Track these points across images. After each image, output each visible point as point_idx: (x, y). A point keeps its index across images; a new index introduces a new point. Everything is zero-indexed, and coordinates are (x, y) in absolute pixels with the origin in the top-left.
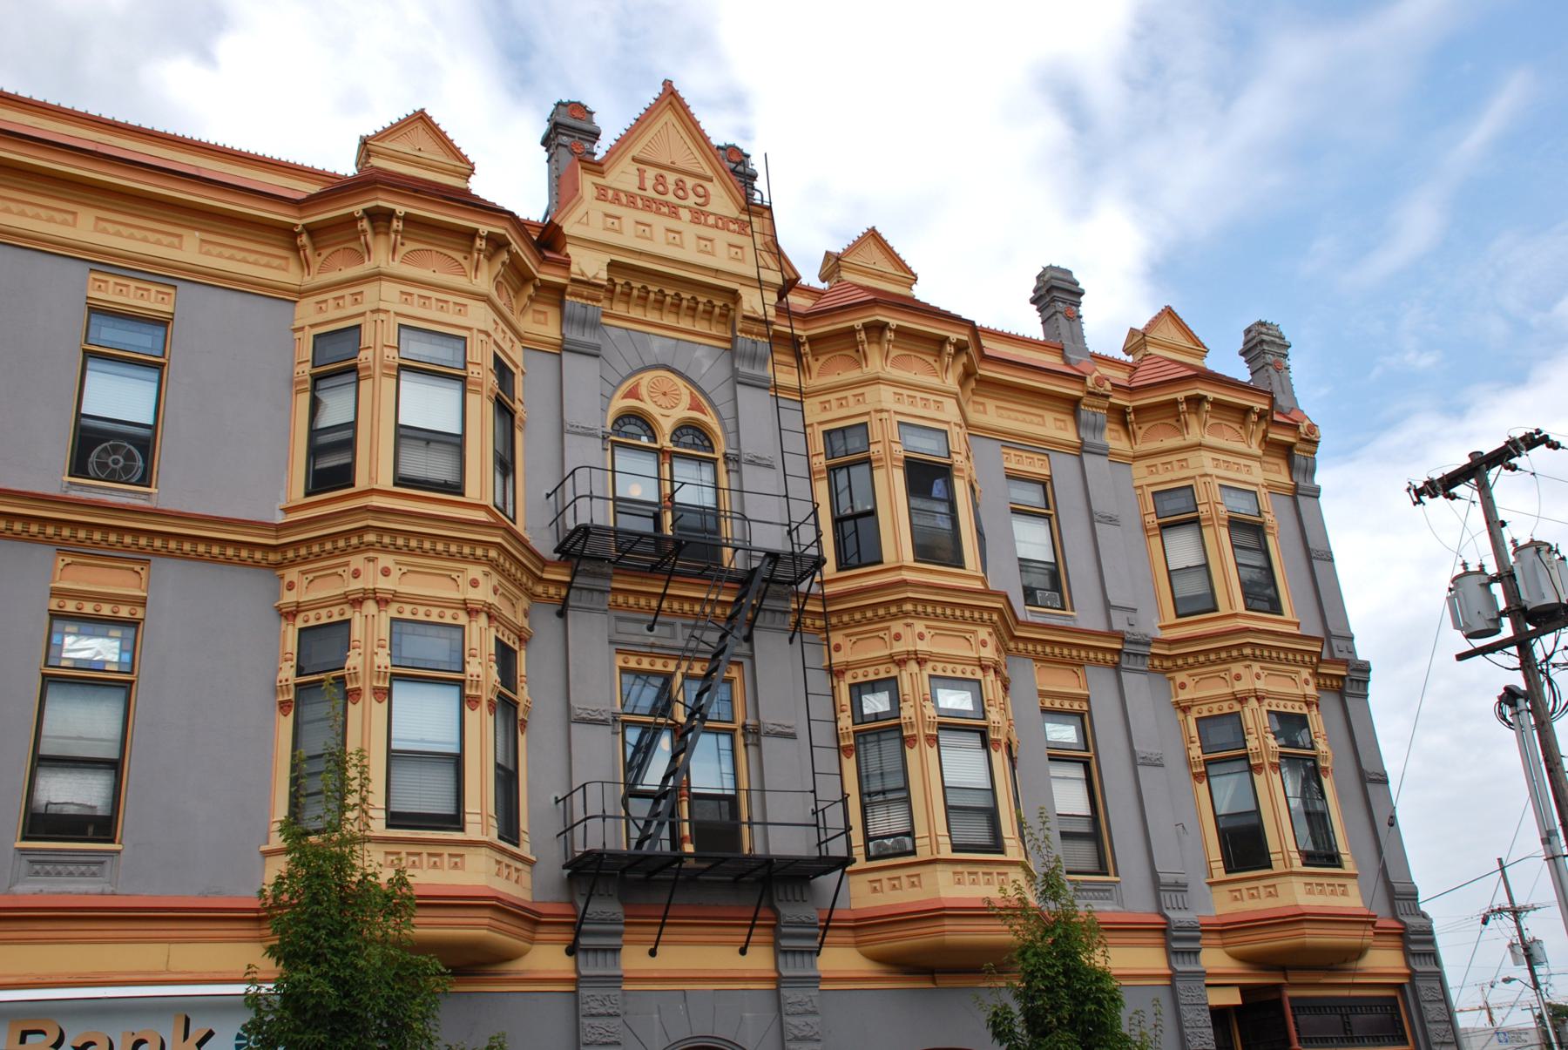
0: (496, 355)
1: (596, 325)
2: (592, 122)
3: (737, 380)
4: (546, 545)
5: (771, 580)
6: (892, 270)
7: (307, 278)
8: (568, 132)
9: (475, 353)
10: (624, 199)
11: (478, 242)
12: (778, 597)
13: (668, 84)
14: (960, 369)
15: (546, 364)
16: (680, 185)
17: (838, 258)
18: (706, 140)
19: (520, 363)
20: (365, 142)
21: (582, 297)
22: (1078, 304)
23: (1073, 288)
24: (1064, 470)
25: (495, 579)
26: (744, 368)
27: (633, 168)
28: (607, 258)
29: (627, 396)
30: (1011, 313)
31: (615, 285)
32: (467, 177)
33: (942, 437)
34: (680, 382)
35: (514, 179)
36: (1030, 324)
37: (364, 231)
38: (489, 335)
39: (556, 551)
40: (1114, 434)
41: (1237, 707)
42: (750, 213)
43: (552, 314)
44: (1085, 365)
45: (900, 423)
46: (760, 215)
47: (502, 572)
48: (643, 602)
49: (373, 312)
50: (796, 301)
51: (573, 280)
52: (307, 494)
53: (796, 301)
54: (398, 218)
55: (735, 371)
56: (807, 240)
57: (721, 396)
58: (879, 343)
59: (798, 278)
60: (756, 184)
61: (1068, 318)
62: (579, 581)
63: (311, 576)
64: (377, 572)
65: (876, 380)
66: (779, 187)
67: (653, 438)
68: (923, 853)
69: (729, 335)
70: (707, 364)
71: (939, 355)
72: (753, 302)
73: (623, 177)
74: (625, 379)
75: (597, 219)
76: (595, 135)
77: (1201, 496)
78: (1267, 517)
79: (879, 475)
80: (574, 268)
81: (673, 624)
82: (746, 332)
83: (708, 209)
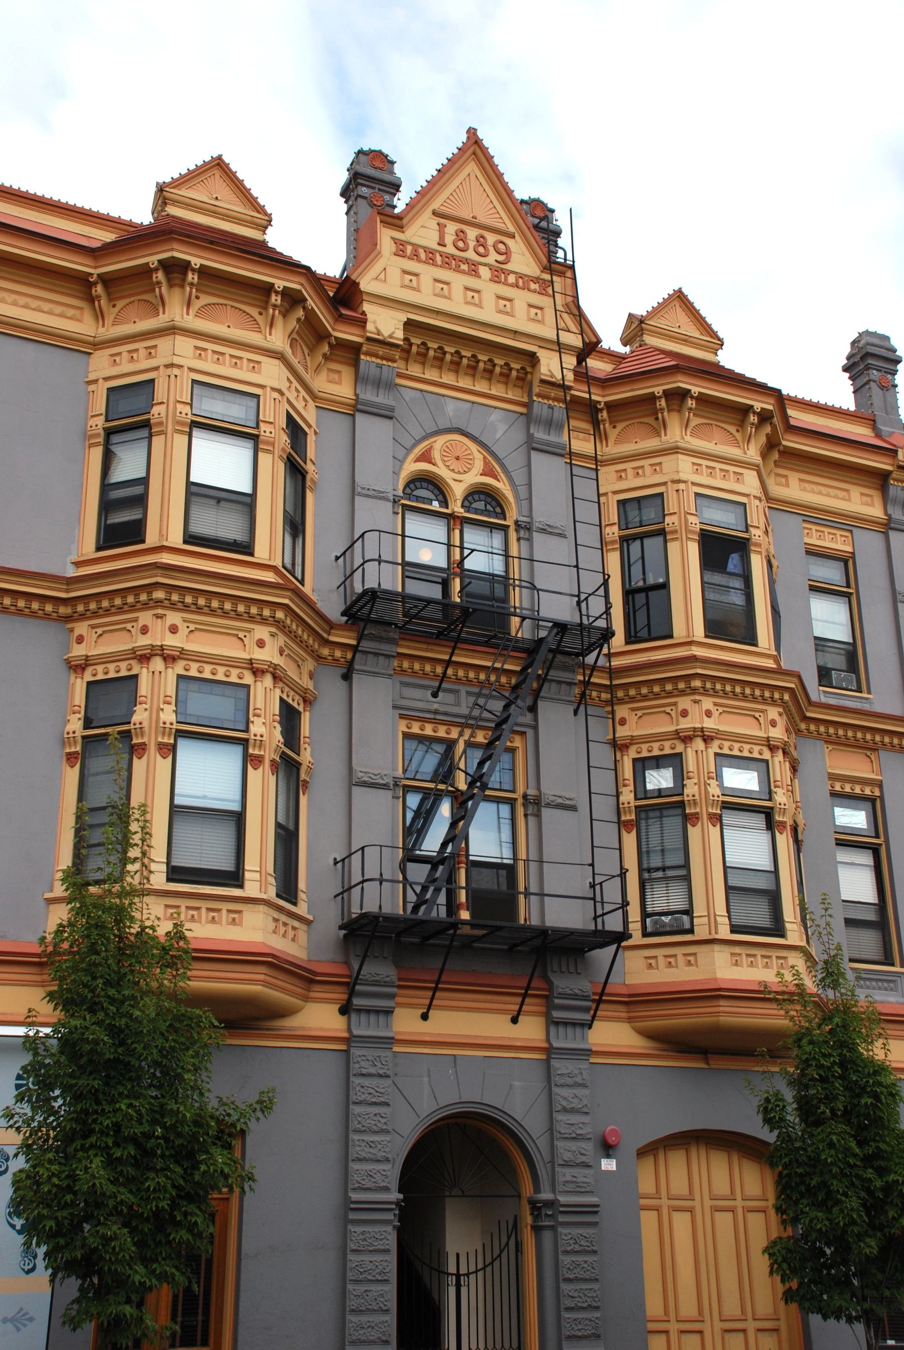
0: (289, 415)
1: (391, 386)
2: (392, 173)
3: (532, 446)
4: (333, 608)
6: (697, 334)
8: (369, 182)
9: (267, 413)
10: (423, 256)
12: (565, 668)
13: (472, 133)
14: (763, 440)
16: (481, 241)
17: (642, 321)
18: (510, 193)
20: (161, 189)
21: (377, 356)
22: (894, 372)
23: (889, 355)
24: (868, 547)
25: (282, 639)
26: (540, 434)
28: (403, 317)
34: (473, 447)
36: (840, 393)
38: (281, 393)
39: (343, 614)
41: (680, 748)
42: (552, 272)
43: (347, 374)
45: (697, 494)
46: (562, 274)
48: (428, 668)
50: (594, 364)
51: (369, 339)
52: (99, 549)
53: (594, 364)
57: (515, 462)
59: (599, 341)
61: (882, 388)
62: (365, 645)
63: (100, 631)
65: (675, 450)
66: (581, 245)
68: (701, 933)
69: (525, 400)
70: (501, 428)
71: (741, 424)
72: (551, 365)
73: (424, 231)
75: (394, 275)
80: (370, 327)
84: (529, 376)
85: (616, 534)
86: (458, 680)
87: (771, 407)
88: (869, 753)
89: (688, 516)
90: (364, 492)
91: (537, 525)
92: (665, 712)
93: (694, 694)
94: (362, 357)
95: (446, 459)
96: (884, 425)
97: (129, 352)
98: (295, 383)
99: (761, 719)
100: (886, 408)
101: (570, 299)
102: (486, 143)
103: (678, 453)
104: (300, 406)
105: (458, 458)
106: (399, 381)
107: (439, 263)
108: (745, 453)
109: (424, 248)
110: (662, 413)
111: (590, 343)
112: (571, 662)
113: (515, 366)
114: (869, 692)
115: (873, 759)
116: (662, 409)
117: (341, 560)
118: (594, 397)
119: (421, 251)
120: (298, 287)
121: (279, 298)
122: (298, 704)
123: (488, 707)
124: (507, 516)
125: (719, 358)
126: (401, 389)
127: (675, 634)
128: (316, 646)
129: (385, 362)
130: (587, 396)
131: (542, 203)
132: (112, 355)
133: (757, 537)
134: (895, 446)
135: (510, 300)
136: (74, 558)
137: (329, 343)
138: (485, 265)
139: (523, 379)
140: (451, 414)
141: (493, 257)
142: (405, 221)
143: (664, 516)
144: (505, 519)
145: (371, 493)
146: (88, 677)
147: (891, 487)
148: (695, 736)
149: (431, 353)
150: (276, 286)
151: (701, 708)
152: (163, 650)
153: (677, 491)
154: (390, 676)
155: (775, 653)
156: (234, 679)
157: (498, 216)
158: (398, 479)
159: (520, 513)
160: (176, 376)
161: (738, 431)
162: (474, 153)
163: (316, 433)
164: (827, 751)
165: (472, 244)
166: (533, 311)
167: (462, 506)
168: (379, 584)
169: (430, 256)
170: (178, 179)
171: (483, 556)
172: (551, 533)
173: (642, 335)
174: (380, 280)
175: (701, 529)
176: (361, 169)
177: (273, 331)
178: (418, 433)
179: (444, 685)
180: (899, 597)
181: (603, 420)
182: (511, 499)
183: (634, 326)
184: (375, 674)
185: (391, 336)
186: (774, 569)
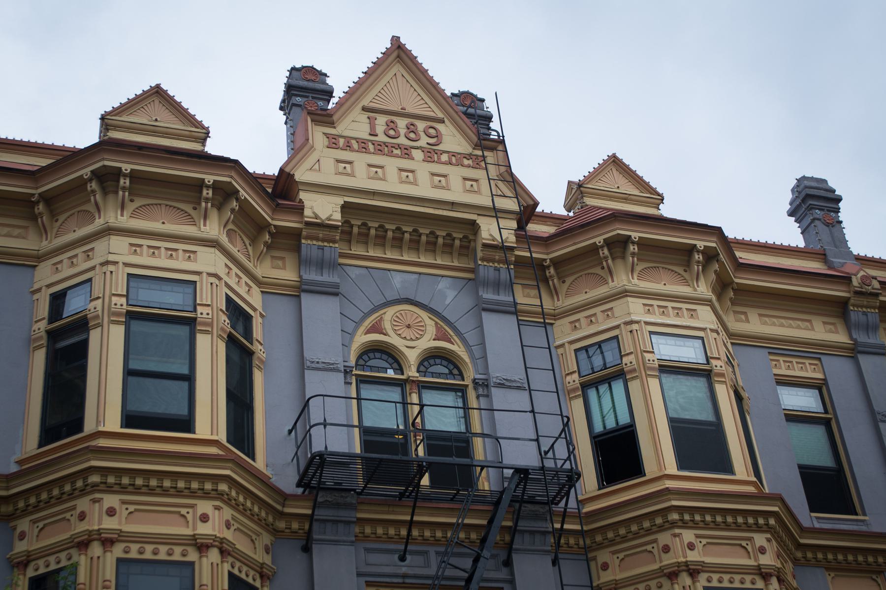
0: (228, 298)
1: (334, 266)
2: (325, 83)
4: (288, 482)
5: (519, 501)
6: (636, 192)
7: (45, 243)
8: (305, 93)
9: (204, 296)
10: (355, 146)
11: (205, 192)
12: (536, 517)
13: (395, 40)
15: (283, 308)
16: (411, 128)
17: (580, 185)
18: (441, 92)
19: (260, 309)
20: (103, 118)
21: (317, 239)
22: (837, 210)
23: (829, 195)
25: (228, 513)
26: (488, 295)
27: (364, 117)
28: (340, 201)
30: (763, 220)
31: (352, 226)
34: (424, 315)
35: (251, 135)
36: (791, 234)
37: (93, 191)
38: (220, 278)
39: (299, 485)
42: (484, 148)
43: (290, 260)
44: (850, 267)
45: (651, 333)
46: (492, 149)
47: (236, 506)
48: (392, 531)
50: (535, 228)
51: (308, 224)
52: (40, 445)
53: (535, 228)
54: (698, 251)
55: (518, 320)
56: (548, 177)
57: (466, 325)
58: (623, 258)
59: (536, 204)
60: (492, 125)
61: (827, 225)
62: (321, 513)
63: (41, 525)
64: (108, 513)
65: (624, 293)
66: (511, 124)
69: (472, 266)
70: (450, 294)
71: (687, 265)
72: (489, 230)
73: (355, 125)
75: (328, 165)
79: (634, 386)
80: (307, 212)
81: (426, 552)
82: (488, 261)
83: (440, 147)
84: (472, 244)
85: (577, 382)
86: (425, 541)
87: (714, 245)
88: (874, 577)
89: (645, 354)
90: (313, 365)
91: (494, 380)
92: (646, 550)
93: (673, 528)
94: (303, 241)
95: (396, 328)
96: (835, 258)
97: (70, 258)
98: (235, 269)
99: (749, 548)
100: (834, 241)
101: (503, 169)
102: (408, 47)
103: (627, 296)
104: (242, 291)
105: (409, 326)
106: (342, 261)
107: (372, 150)
108: (695, 290)
109: (355, 139)
110: (607, 261)
111: (528, 206)
112: (541, 510)
114: (864, 514)
115: (880, 582)
116: (606, 258)
117: (293, 433)
118: (534, 255)
119: (354, 142)
120: (228, 179)
121: (210, 192)
122: (254, 580)
123: (450, 562)
124: (465, 376)
125: (660, 212)
126: (346, 268)
128: (270, 519)
129: (326, 244)
131: (472, 94)
132: (54, 264)
135: (445, 176)
136: (18, 456)
138: (417, 148)
139: (468, 248)
140: (398, 286)
141: (424, 141)
142: (335, 118)
143: (621, 357)
144: (463, 380)
145: (320, 366)
146: (31, 573)
148: (680, 571)
149: (373, 232)
150: (206, 181)
151: (682, 541)
152: (100, 534)
153: (631, 332)
154: (352, 543)
155: (755, 479)
156: (177, 557)
157: (426, 106)
158: (349, 353)
159: (477, 371)
160: (111, 272)
161: (685, 271)
162: (398, 56)
163: (262, 316)
164: (829, 578)
165: (403, 131)
166: (469, 183)
167: (418, 371)
168: (326, 447)
169: (363, 146)
170: (118, 108)
171: (443, 417)
172: (510, 387)
173: (582, 197)
174: (315, 170)
175: (660, 365)
176: (294, 82)
177: (615, 279)
178: (367, 307)
179: (409, 547)
180: (879, 417)
181: (551, 276)
182: (466, 358)
183: (574, 191)
184: (336, 542)
185: (329, 219)
186: (745, 402)
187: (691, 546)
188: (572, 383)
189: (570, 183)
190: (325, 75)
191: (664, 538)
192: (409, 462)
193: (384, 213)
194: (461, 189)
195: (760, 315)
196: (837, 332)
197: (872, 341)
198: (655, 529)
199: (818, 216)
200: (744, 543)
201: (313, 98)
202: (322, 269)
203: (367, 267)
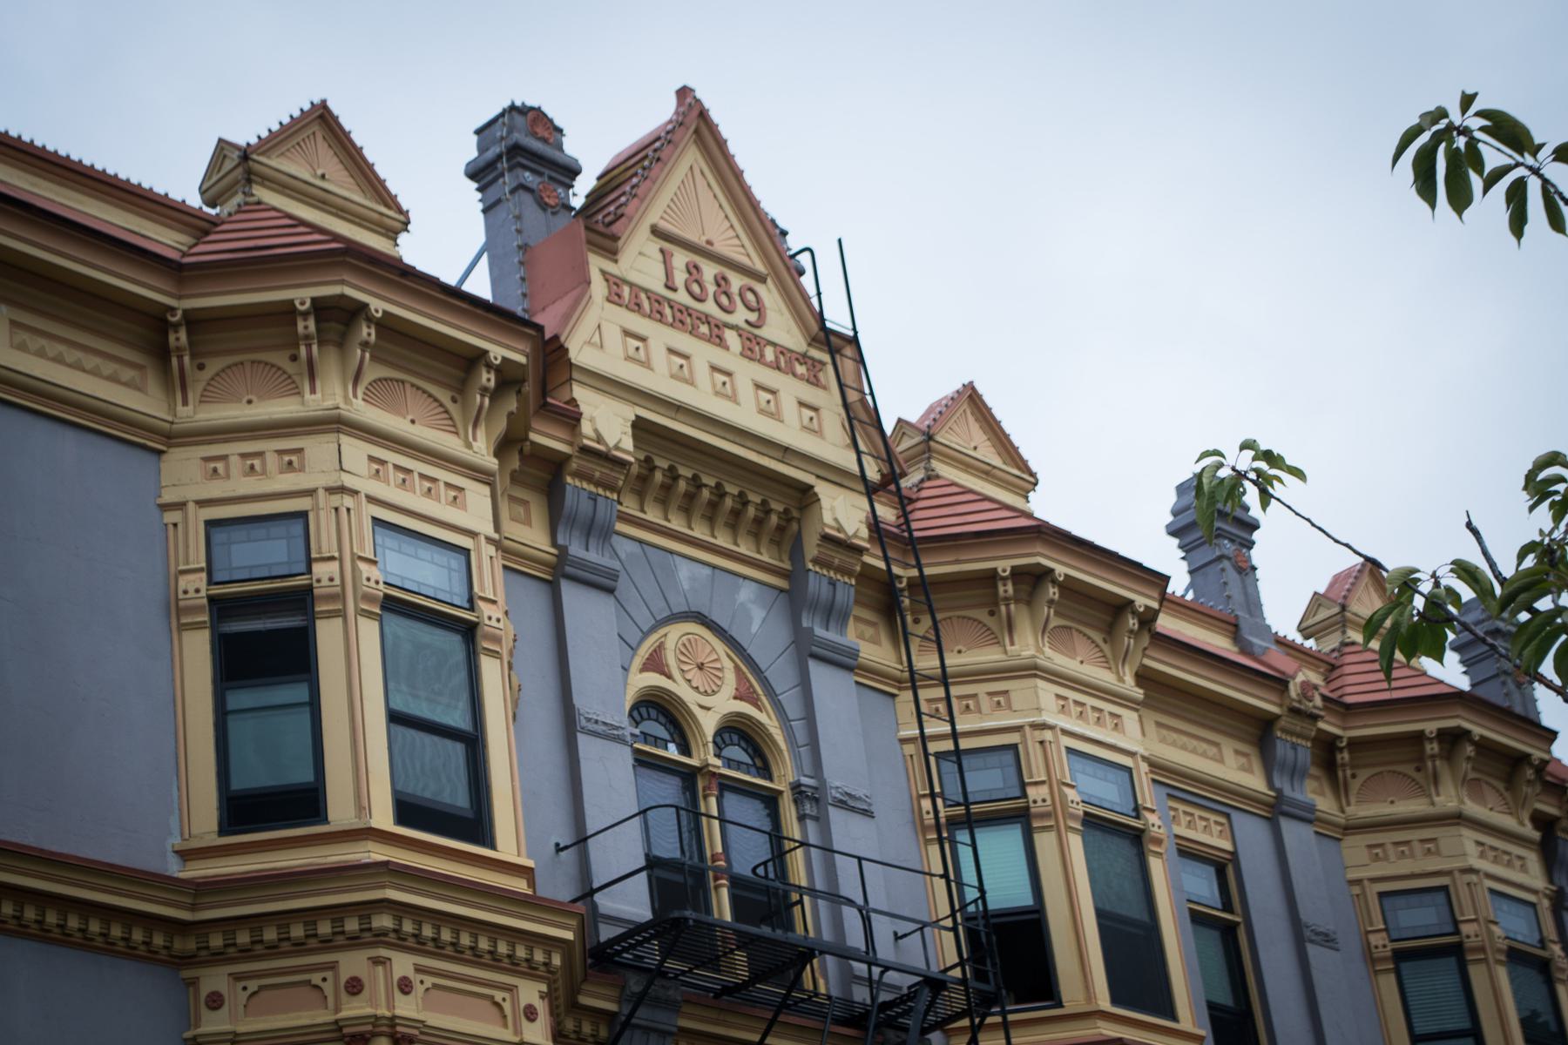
2: (560, 148)
3: (806, 651)
6: (357, 197)
14: (501, 426)
17: (246, 154)
21: (590, 479)
27: (654, 247)
29: (645, 668)
31: (653, 469)
32: (392, 234)
33: (456, 561)
34: (720, 647)
40: (869, 631)
45: (377, 521)
49: (331, 490)
51: (585, 450)
54: (489, 366)
57: (782, 676)
65: (1032, 671)
67: (685, 749)
69: (787, 566)
70: (758, 615)
71: (460, 389)
72: (844, 512)
74: (646, 635)
76: (571, 171)
77: (1035, 768)
78: (1152, 819)
80: (586, 428)
84: (795, 526)
85: (203, 593)
87: (522, 359)
90: (591, 726)
95: (686, 668)
99: (507, 1006)
105: (701, 667)
106: (620, 527)
107: (670, 320)
108: (469, 446)
113: (777, 506)
127: (331, 817)
129: (601, 491)
130: (882, 565)
133: (372, 584)
134: (1283, 673)
136: (175, 841)
137: (521, 451)
141: (741, 316)
143: (309, 562)
145: (600, 728)
147: (1279, 743)
151: (389, 974)
153: (1042, 743)
157: (736, 242)
159: (799, 768)
161: (454, 400)
172: (853, 809)
175: (1086, 813)
177: (1016, 638)
180: (1307, 933)
181: (178, 349)
183: (228, 165)
185: (617, 447)
187: (405, 986)
188: (192, 594)
189: (222, 144)
190: (560, 131)
191: (353, 963)
192: (712, 926)
193: (682, 445)
194: (797, 424)
195: (13, 323)
196: (1249, 770)
197: (831, 635)
198: (340, 940)
199: (1226, 552)
200: (499, 995)
201: (551, 178)
202: (588, 535)
203: (641, 542)
